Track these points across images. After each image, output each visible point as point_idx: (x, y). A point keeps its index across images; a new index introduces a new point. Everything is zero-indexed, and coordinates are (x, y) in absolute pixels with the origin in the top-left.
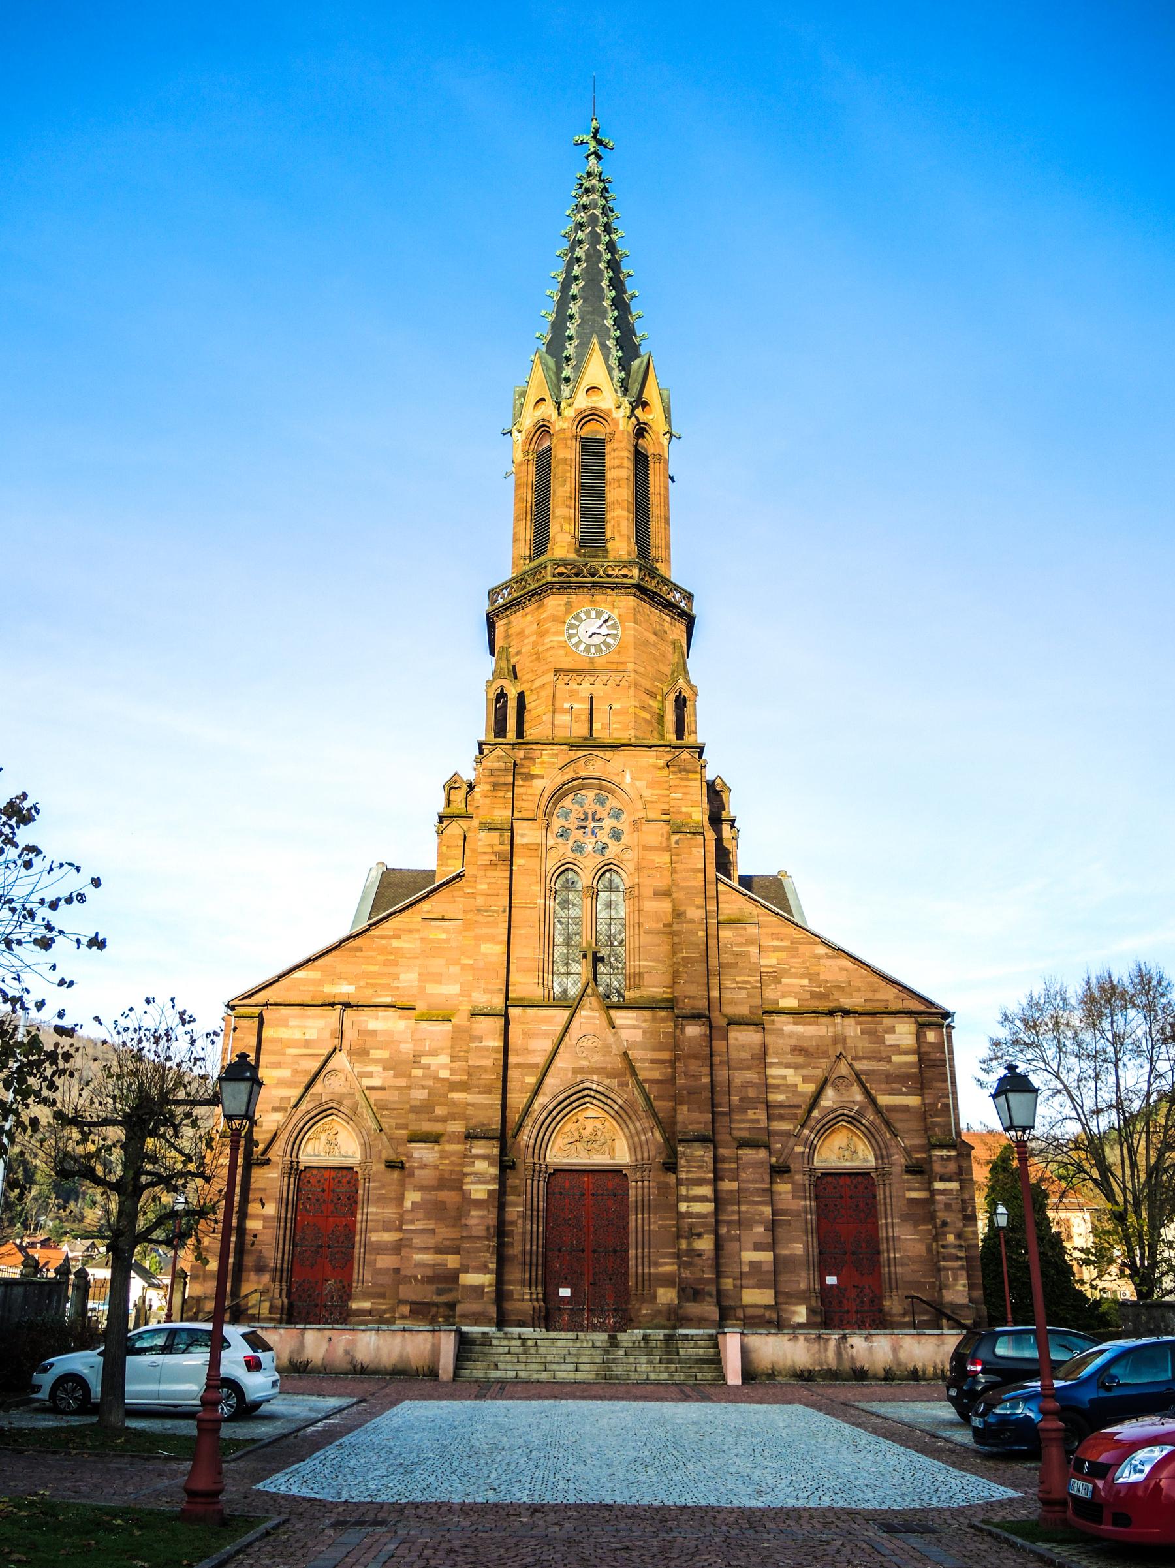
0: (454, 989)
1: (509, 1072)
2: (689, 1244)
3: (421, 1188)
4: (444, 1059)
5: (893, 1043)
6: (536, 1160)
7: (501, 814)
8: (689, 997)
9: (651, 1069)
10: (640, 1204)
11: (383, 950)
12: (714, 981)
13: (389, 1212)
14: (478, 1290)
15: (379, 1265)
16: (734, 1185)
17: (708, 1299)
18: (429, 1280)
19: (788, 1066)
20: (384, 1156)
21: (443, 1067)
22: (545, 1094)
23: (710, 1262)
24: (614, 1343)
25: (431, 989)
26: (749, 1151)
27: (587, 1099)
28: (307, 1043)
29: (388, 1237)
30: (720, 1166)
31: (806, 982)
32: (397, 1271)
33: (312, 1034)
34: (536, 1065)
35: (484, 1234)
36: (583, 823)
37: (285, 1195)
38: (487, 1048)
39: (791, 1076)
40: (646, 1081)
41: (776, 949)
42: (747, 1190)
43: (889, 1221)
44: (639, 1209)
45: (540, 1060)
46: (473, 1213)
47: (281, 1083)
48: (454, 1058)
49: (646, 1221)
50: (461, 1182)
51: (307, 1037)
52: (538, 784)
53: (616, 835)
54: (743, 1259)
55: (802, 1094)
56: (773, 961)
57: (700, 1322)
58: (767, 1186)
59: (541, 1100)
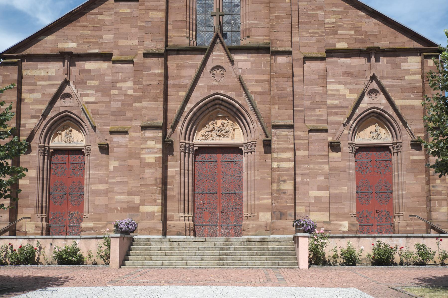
0: (135, 42)
1: (169, 90)
2: (278, 186)
3: (118, 159)
4: (130, 84)
5: (406, 68)
6: (187, 141)
8: (280, 40)
9: (256, 85)
10: (249, 165)
11: (92, 21)
12: (295, 31)
13: (102, 173)
14: (150, 215)
15: (97, 203)
16: (306, 153)
17: (289, 217)
18: (125, 210)
19: (340, 83)
20: (98, 141)
21: (130, 88)
22: (191, 103)
23: (291, 196)
24: (228, 244)
25: (122, 42)
27: (217, 106)
28: (50, 78)
29: (101, 187)
31: (353, 32)
32: (106, 205)
33: (52, 72)
34: (186, 85)
35: (153, 182)
37: (41, 165)
38: (154, 74)
39: (342, 89)
40: (252, 93)
41: (335, 13)
42: (314, 155)
43: (400, 173)
44: (249, 168)
45: (189, 82)
46: (147, 171)
47: (36, 101)
48: (135, 82)
49: (253, 175)
50: (140, 154)
51: (50, 74)
54: (310, 195)
55: (348, 100)
56: (333, 20)
57: (285, 231)
58: (326, 153)
59: (190, 106)
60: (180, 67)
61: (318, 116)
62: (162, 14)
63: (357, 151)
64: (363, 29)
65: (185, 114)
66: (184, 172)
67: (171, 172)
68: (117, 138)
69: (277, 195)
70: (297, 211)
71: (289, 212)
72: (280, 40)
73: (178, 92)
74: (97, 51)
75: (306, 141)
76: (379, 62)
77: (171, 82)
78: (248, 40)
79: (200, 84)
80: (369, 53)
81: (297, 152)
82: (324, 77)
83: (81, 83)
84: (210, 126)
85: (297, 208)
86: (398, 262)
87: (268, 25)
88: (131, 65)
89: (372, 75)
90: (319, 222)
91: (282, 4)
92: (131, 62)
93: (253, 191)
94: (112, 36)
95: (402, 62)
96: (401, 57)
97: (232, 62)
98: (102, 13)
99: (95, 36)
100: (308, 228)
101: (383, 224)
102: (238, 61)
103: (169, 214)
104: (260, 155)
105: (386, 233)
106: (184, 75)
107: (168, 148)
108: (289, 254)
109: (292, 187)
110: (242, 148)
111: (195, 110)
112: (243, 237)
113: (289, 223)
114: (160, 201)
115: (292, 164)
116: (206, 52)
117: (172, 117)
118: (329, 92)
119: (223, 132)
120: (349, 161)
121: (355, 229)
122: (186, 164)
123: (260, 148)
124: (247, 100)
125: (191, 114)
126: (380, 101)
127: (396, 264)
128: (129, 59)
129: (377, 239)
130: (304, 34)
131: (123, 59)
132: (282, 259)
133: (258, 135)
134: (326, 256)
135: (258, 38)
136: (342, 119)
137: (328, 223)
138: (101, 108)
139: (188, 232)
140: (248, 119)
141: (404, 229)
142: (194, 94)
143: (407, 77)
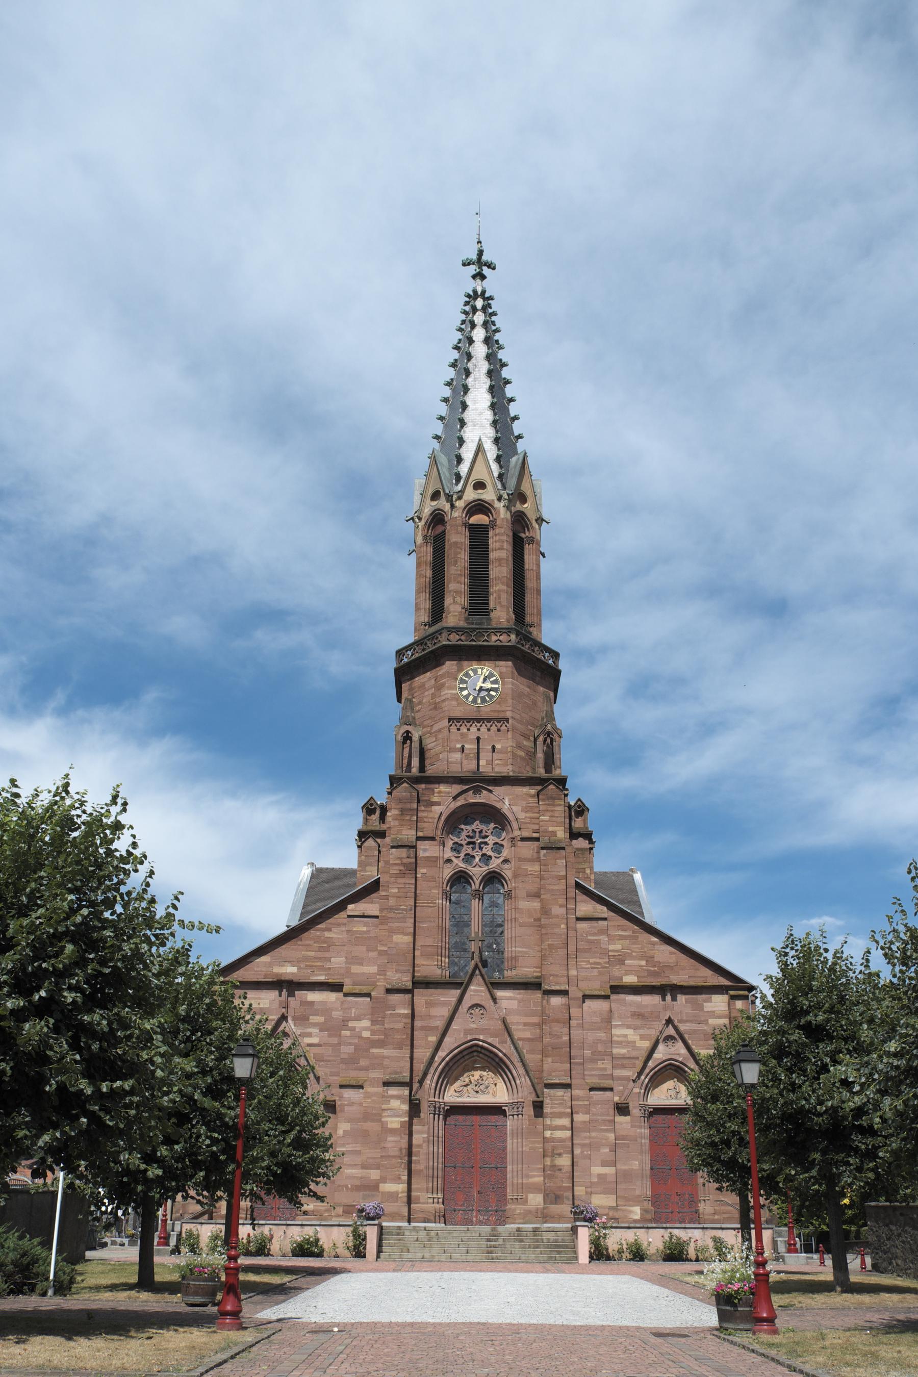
0: (373, 969)
2: (552, 1161)
3: (349, 1120)
4: (366, 1023)
5: (710, 1009)
6: (436, 1100)
7: (408, 835)
8: (553, 975)
9: (524, 1030)
12: (572, 962)
14: (393, 1196)
16: (586, 1118)
18: (357, 1188)
19: (629, 1027)
21: (366, 1029)
22: (443, 1050)
24: (495, 1235)
25: (356, 969)
27: (475, 1054)
31: (643, 963)
35: (397, 1153)
38: (400, 1015)
40: (520, 1039)
41: (622, 938)
42: (597, 1121)
45: (440, 1024)
46: (389, 1139)
48: (374, 1022)
49: (520, 1144)
51: (261, 1006)
52: (437, 809)
53: (498, 848)
55: (639, 1049)
56: (619, 947)
57: (560, 1218)
59: (441, 1054)
60: (430, 1004)
61: (601, 1069)
62: (409, 939)
63: (651, 1114)
64: (656, 959)
65: (435, 1065)
66: (432, 1139)
67: (417, 1139)
68: (348, 1094)
69: (550, 1172)
70: (576, 1193)
71: (566, 1194)
72: (553, 975)
73: (427, 1036)
74: (322, 978)
75: (586, 1103)
76: (676, 1000)
77: (418, 1024)
78: (514, 972)
79: (454, 1026)
80: (662, 990)
81: (575, 1116)
82: (608, 1020)
83: (302, 1019)
84: (465, 1079)
85: (575, 1188)
86: (694, 1258)
87: (539, 954)
88: (368, 999)
89: (667, 1018)
90: (603, 1207)
91: (557, 930)
92: (368, 995)
93: (520, 1166)
94: (343, 959)
95: (705, 1001)
96: (703, 996)
97: (494, 1000)
98: (329, 930)
99: (320, 959)
100: (589, 1215)
101: (685, 1210)
102: (502, 998)
103: (413, 1194)
104: (530, 1120)
105: (689, 1223)
106: (435, 1014)
107: (415, 1109)
108: (566, 1247)
109: (569, 1163)
110: (506, 1108)
111: (447, 1059)
112: (507, 1226)
113: (565, 1208)
114: (405, 1178)
115: (569, 1133)
116: (462, 986)
117: (419, 1067)
118: (615, 1038)
119: (482, 1087)
120: (641, 1127)
121: (649, 1217)
122: (436, 1128)
123: (529, 1111)
124: (512, 1048)
125: (443, 1064)
126: (679, 1050)
127: (691, 1260)
128: (365, 991)
129: (669, 1230)
130: (584, 964)
131: (357, 991)
132: (559, 1253)
133: (526, 1093)
134: (610, 1251)
135: (526, 970)
136: (631, 1073)
137: (614, 1209)
138: (327, 1052)
139: (437, 1218)
140: (514, 1072)
141: (711, 1217)
142: (447, 1039)
143: (711, 1021)
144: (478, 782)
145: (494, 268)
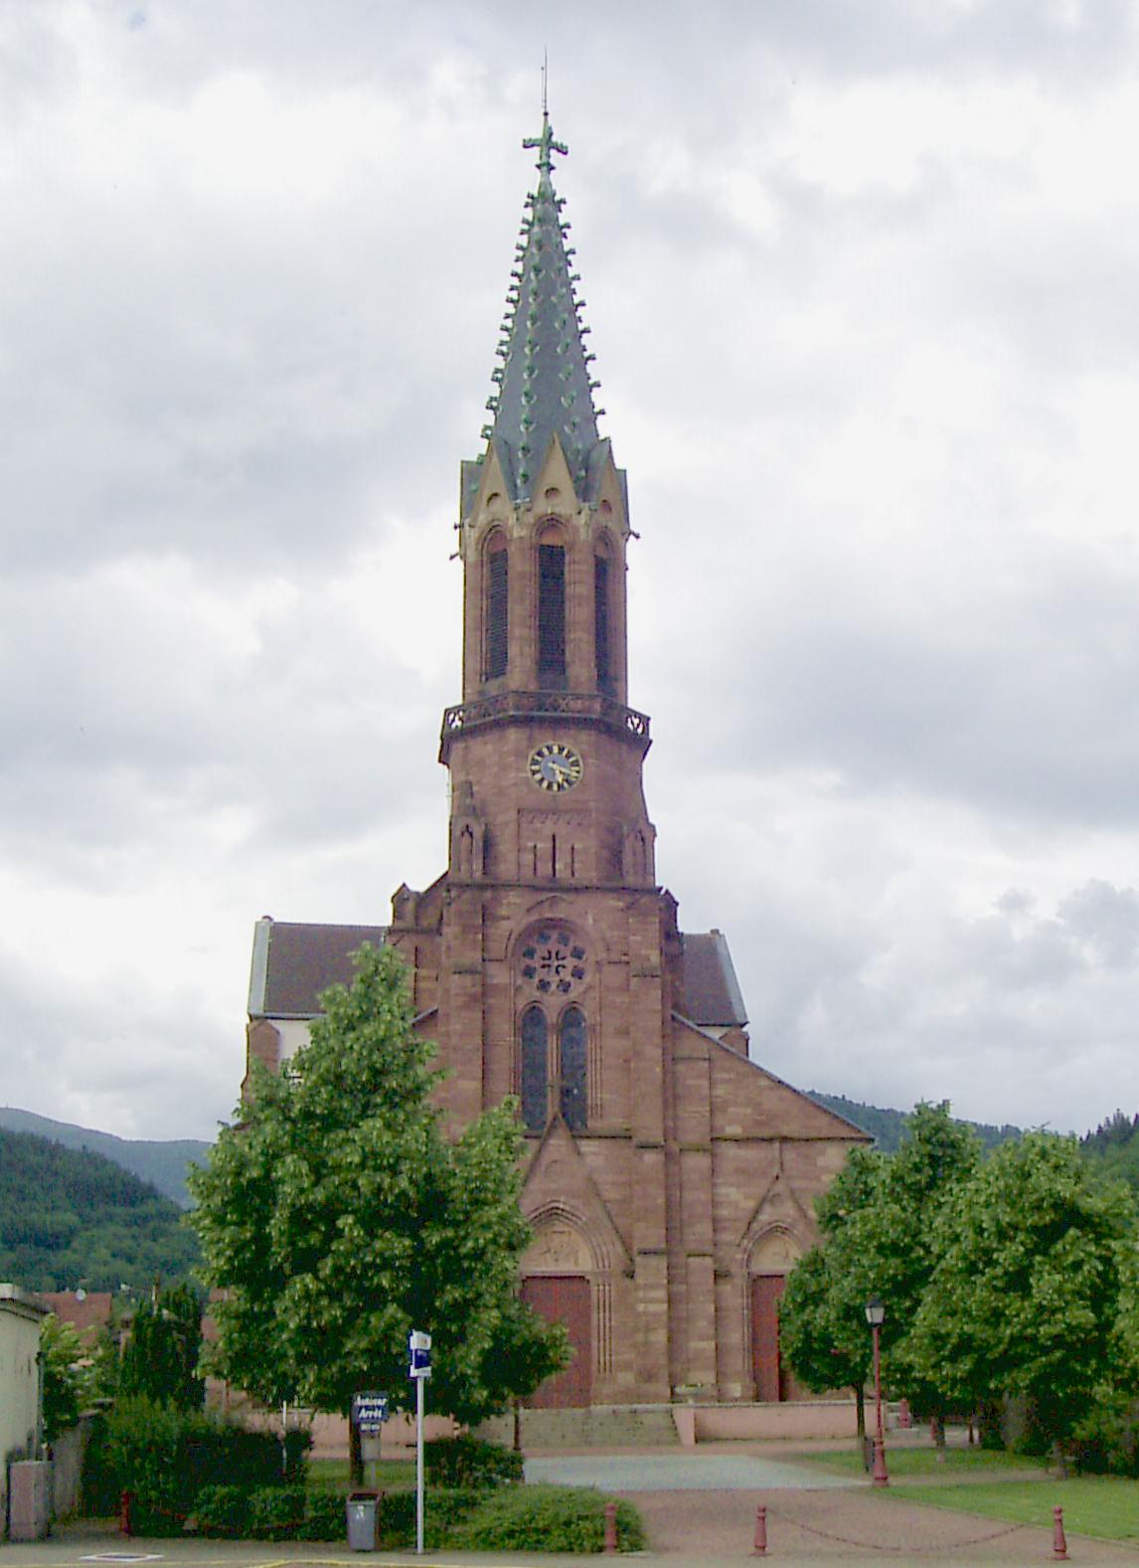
7: (473, 957)
26: (698, 1260)
30: (673, 1272)
31: (749, 1111)
36: (547, 962)
52: (505, 925)
53: (578, 974)
57: (656, 1398)
135: (614, 1122)
144: (554, 887)
145: (565, 153)
